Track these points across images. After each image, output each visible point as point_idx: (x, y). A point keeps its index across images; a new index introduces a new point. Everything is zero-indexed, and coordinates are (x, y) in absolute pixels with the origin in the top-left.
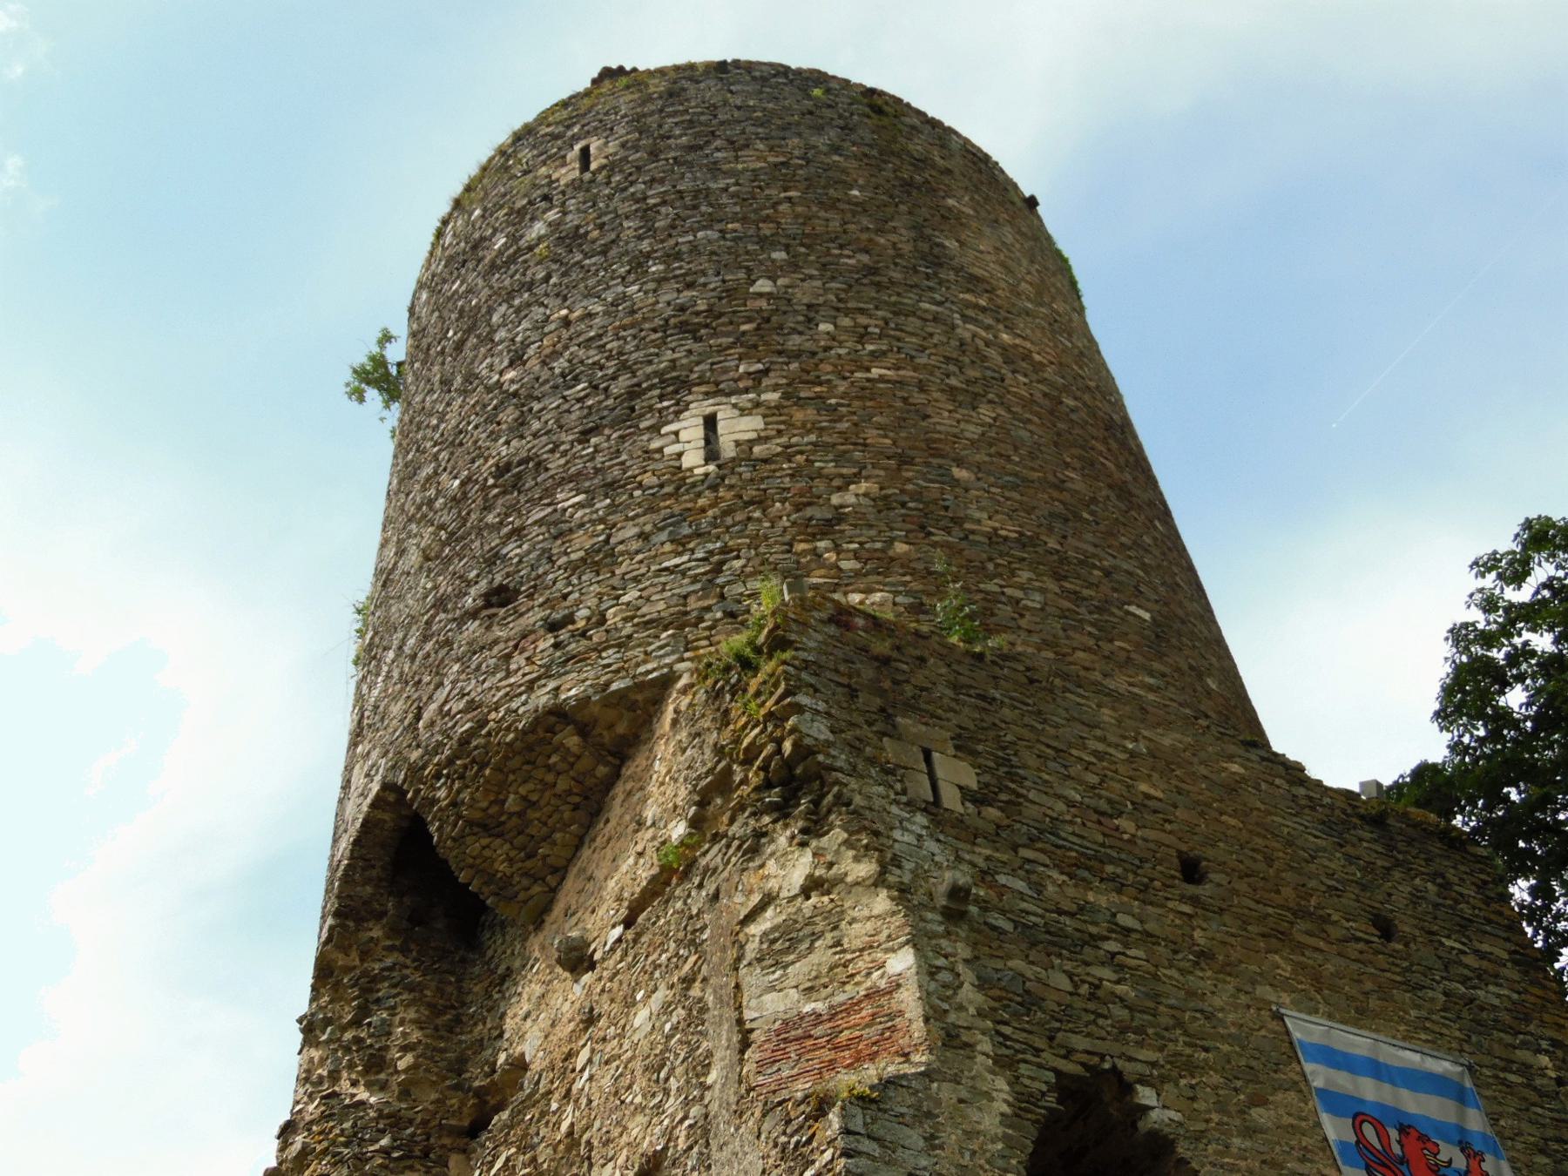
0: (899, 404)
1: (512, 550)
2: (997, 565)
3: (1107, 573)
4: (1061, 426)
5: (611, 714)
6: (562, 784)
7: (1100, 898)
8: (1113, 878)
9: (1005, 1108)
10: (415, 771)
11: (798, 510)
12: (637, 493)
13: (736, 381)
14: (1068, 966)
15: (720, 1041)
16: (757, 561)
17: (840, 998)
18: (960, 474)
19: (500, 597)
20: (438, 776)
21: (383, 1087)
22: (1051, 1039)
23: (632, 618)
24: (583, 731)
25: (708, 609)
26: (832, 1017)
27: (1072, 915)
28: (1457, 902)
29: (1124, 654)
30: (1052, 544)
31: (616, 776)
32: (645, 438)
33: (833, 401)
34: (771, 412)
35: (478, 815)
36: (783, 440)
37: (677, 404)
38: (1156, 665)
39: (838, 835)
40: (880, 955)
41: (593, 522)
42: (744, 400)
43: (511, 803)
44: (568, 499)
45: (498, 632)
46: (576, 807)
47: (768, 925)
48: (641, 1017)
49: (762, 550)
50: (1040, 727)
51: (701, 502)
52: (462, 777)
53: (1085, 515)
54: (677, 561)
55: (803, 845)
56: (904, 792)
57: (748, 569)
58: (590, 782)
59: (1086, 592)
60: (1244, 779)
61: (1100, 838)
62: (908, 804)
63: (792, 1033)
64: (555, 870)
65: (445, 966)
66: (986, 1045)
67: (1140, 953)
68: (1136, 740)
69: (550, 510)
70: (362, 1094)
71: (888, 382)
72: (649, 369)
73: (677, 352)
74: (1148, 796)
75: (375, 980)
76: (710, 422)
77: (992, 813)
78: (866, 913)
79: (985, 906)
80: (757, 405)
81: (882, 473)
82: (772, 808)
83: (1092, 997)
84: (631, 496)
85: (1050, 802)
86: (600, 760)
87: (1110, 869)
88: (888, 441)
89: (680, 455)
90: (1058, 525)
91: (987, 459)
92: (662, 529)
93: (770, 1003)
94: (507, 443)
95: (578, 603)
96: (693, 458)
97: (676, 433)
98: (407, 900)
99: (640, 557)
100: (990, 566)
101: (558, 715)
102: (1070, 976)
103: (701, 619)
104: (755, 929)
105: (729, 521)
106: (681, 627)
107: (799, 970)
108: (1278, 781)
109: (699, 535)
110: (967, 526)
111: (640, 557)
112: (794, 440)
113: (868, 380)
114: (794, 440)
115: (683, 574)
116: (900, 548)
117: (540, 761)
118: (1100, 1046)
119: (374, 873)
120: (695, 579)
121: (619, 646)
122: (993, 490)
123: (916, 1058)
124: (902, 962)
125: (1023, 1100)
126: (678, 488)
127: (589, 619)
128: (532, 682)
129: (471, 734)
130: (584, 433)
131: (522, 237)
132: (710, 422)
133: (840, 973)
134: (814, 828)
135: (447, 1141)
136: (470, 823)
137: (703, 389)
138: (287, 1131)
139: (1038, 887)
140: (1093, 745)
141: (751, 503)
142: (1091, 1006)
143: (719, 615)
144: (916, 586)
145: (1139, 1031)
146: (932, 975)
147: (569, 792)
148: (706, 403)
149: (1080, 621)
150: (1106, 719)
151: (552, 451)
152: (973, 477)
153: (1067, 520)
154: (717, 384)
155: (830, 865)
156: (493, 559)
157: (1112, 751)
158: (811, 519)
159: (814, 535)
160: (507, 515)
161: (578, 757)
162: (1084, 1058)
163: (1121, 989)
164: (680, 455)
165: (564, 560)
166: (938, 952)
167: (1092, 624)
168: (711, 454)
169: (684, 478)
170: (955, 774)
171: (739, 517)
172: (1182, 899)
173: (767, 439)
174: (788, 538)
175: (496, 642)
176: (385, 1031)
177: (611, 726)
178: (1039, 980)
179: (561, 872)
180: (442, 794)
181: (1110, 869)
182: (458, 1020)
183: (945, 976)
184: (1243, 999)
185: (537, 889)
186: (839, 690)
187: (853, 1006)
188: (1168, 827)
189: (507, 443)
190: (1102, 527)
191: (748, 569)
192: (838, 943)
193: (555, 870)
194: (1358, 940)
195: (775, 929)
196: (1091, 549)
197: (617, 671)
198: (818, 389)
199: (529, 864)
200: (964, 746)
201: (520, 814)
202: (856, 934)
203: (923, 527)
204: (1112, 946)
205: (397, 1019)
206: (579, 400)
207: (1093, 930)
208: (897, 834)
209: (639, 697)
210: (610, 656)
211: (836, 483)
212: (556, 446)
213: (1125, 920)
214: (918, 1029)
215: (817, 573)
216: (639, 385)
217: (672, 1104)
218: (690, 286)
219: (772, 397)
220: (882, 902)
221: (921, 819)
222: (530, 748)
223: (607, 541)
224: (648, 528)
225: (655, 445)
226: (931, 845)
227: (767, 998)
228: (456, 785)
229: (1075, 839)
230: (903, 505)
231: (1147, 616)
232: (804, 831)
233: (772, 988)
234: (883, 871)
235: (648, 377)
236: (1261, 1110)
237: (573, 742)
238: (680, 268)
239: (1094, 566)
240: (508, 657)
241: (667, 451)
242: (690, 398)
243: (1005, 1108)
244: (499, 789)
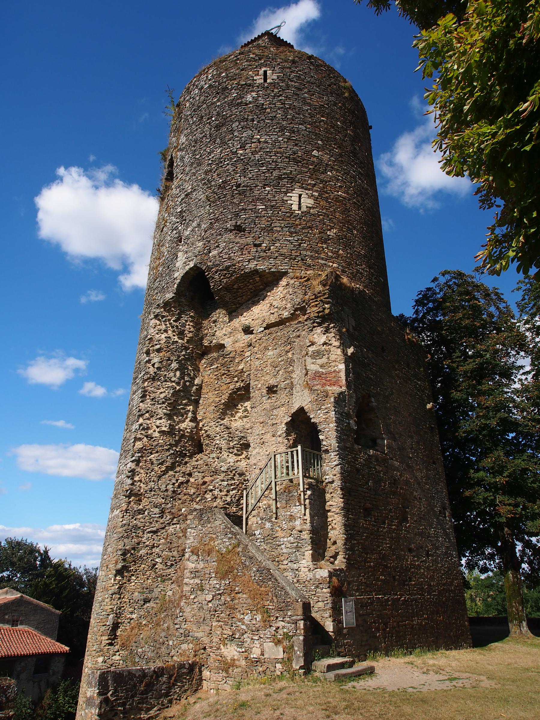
16: (309, 246)
23: (278, 251)
32: (283, 195)
34: (316, 199)
36: (318, 210)
40: (337, 363)
47: (314, 349)
52: (224, 276)
55: (324, 334)
69: (254, 207)
72: (285, 171)
73: (291, 168)
78: (335, 353)
82: (317, 323)
92: (287, 227)
93: (313, 367)
96: (295, 207)
99: (280, 234)
101: (256, 272)
103: (295, 259)
105: (304, 231)
107: (320, 361)
109: (296, 233)
115: (292, 243)
120: (294, 246)
121: (274, 258)
123: (343, 388)
124: (342, 367)
126: (291, 215)
127: (266, 247)
129: (230, 266)
131: (243, 97)
134: (327, 331)
143: (300, 259)
147: (251, 289)
151: (255, 187)
154: (302, 184)
161: (257, 282)
169: (293, 213)
173: (314, 208)
176: (184, 325)
179: (241, 304)
187: (330, 373)
191: (307, 248)
195: (315, 351)
197: (274, 266)
205: (187, 324)
206: (263, 173)
214: (344, 382)
218: (296, 145)
224: (283, 225)
225: (285, 198)
228: (222, 277)
232: (325, 331)
233: (313, 363)
235: (284, 174)
237: (257, 279)
238: (294, 137)
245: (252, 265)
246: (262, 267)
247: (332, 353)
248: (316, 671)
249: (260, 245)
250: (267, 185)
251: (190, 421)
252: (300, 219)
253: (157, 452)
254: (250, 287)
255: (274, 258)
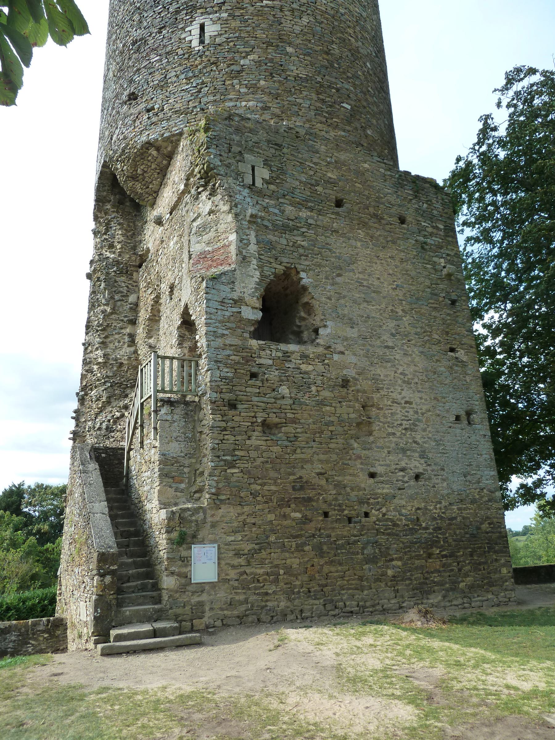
0: (271, 18)
1: (137, 78)
2: (296, 89)
3: (338, 90)
4: (336, 23)
5: (165, 144)
6: (153, 166)
7: (304, 214)
8: (309, 208)
9: (258, 280)
10: (111, 158)
11: (228, 67)
12: (176, 57)
13: (212, 7)
14: (287, 236)
15: (185, 256)
17: (216, 247)
18: (290, 50)
19: (133, 97)
20: (118, 161)
21: (114, 253)
22: (276, 259)
24: (158, 149)
25: (195, 107)
26: (213, 252)
27: (292, 220)
28: (432, 210)
29: (336, 124)
30: (319, 79)
31: (169, 164)
33: (246, 17)
35: (130, 174)
36: (226, 36)
37: (191, 18)
38: (348, 128)
39: (219, 197)
41: (162, 69)
42: (214, 16)
43: (139, 171)
44: (154, 58)
45: (132, 111)
46: (158, 173)
48: (172, 243)
49: (214, 84)
50: (296, 154)
51: (197, 62)
53: (336, 65)
54: (187, 87)
55: (209, 199)
56: (243, 181)
57: (209, 92)
58: (161, 166)
59: (327, 99)
60: (368, 170)
61: (309, 194)
62: (243, 185)
63: (203, 256)
64: (155, 192)
65: (130, 217)
66: (255, 262)
67: (313, 232)
68: (331, 158)
70: (108, 254)
71: (268, 7)
74: (330, 178)
75: (109, 221)
76: (202, 27)
77: (272, 187)
79: (263, 219)
80: (219, 19)
81: (260, 50)
82: (202, 186)
83: (293, 246)
84: (174, 59)
85: (294, 182)
86: (164, 159)
87: (310, 204)
88: (265, 36)
89: (191, 41)
90: (323, 71)
91: (301, 42)
92: (183, 73)
94: (136, 30)
95: (155, 102)
96: (195, 43)
97: (190, 31)
98: (117, 196)
99: (175, 85)
100: (293, 90)
101: (149, 144)
102: (287, 239)
104: (195, 224)
105: (205, 71)
106: (186, 114)
107: (206, 238)
108: (381, 170)
110: (288, 73)
111: (175, 85)
112: (231, 35)
113: (262, 6)
114: (231, 35)
116: (262, 83)
117: (146, 158)
118: (291, 261)
119: (106, 188)
122: (301, 56)
124: (233, 237)
125: (263, 276)
128: (142, 131)
129: (125, 147)
130: (160, 28)
132: (202, 27)
133: (217, 238)
134: (213, 193)
135: (132, 269)
136: (128, 177)
137: (201, 11)
138: (92, 262)
139: (283, 212)
140: (315, 160)
141: (212, 64)
142: (292, 249)
143: (199, 110)
144: (265, 99)
145: (307, 256)
146: (241, 241)
147: (156, 169)
148: (201, 18)
149: (322, 111)
150: (322, 150)
151: (150, 36)
152: (294, 51)
153: (327, 68)
155: (217, 206)
156: (131, 81)
157: (321, 162)
158: (232, 71)
159: (233, 78)
160: (136, 63)
162: (285, 264)
163: (303, 243)
164: (191, 41)
165: (152, 83)
166: (245, 234)
167: (327, 113)
168: (202, 42)
170: (263, 173)
171: (208, 69)
172: (333, 213)
174: (223, 79)
175: (131, 115)
177: (166, 148)
178: (276, 241)
180: (119, 166)
181: (310, 204)
182: (134, 234)
183: (245, 241)
184: (344, 245)
185: (150, 198)
186: (226, 145)
188: (335, 188)
189: (136, 30)
190: (341, 70)
192: (217, 230)
193: (155, 192)
194: (391, 224)
196: (334, 80)
198: (242, 11)
199: (147, 190)
200: (266, 163)
201: (143, 174)
202: (222, 227)
203: (271, 74)
204: (304, 230)
207: (298, 225)
208: (237, 196)
209: (174, 139)
210: (165, 124)
211: (243, 55)
212: (151, 34)
213: (310, 221)
215: (232, 93)
216: (179, 8)
217: (176, 270)
219: (225, 15)
220: (230, 218)
221: (247, 191)
222: (142, 154)
223: (165, 77)
224: (178, 73)
226: (248, 200)
227: (197, 245)
229: (301, 195)
230: (266, 64)
231: (349, 107)
232: (210, 194)
233: (198, 242)
234: (231, 209)
236: (340, 278)
237: (155, 153)
239: (333, 88)
240: (135, 121)
241: (187, 39)
242: (196, 15)
243: (258, 280)
244: (135, 166)
245: (144, 138)
246: (153, 135)
247: (221, 222)
248: (444, 597)
249: (153, 108)
250: (163, 28)
251: (129, 346)
252: (201, 56)
253: (96, 387)
254: (153, 167)
255: (167, 120)
